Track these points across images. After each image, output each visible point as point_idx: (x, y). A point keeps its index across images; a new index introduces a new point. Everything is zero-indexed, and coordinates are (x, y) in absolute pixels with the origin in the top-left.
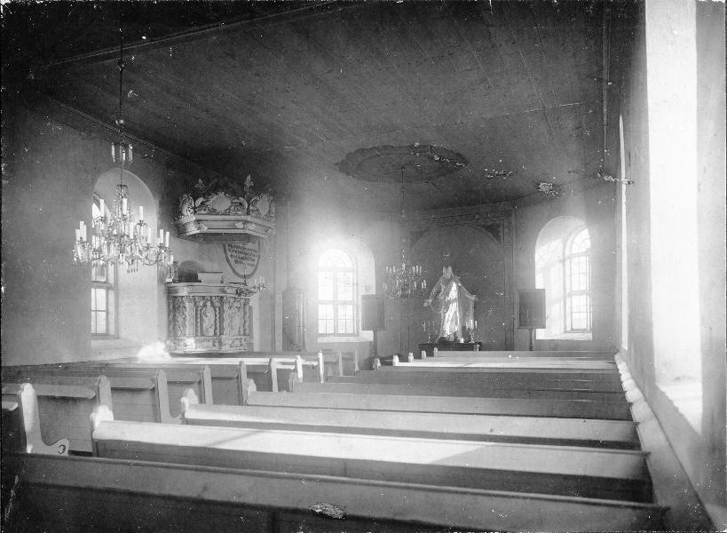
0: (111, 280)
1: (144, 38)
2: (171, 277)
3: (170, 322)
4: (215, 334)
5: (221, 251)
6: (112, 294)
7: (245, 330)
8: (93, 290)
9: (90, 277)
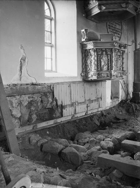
0: (53, 43)
1: (56, 163)
2: (84, 38)
3: (83, 69)
4: (108, 69)
5: (105, 27)
6: (53, 49)
7: (123, 68)
8: (45, 47)
9: (44, 41)
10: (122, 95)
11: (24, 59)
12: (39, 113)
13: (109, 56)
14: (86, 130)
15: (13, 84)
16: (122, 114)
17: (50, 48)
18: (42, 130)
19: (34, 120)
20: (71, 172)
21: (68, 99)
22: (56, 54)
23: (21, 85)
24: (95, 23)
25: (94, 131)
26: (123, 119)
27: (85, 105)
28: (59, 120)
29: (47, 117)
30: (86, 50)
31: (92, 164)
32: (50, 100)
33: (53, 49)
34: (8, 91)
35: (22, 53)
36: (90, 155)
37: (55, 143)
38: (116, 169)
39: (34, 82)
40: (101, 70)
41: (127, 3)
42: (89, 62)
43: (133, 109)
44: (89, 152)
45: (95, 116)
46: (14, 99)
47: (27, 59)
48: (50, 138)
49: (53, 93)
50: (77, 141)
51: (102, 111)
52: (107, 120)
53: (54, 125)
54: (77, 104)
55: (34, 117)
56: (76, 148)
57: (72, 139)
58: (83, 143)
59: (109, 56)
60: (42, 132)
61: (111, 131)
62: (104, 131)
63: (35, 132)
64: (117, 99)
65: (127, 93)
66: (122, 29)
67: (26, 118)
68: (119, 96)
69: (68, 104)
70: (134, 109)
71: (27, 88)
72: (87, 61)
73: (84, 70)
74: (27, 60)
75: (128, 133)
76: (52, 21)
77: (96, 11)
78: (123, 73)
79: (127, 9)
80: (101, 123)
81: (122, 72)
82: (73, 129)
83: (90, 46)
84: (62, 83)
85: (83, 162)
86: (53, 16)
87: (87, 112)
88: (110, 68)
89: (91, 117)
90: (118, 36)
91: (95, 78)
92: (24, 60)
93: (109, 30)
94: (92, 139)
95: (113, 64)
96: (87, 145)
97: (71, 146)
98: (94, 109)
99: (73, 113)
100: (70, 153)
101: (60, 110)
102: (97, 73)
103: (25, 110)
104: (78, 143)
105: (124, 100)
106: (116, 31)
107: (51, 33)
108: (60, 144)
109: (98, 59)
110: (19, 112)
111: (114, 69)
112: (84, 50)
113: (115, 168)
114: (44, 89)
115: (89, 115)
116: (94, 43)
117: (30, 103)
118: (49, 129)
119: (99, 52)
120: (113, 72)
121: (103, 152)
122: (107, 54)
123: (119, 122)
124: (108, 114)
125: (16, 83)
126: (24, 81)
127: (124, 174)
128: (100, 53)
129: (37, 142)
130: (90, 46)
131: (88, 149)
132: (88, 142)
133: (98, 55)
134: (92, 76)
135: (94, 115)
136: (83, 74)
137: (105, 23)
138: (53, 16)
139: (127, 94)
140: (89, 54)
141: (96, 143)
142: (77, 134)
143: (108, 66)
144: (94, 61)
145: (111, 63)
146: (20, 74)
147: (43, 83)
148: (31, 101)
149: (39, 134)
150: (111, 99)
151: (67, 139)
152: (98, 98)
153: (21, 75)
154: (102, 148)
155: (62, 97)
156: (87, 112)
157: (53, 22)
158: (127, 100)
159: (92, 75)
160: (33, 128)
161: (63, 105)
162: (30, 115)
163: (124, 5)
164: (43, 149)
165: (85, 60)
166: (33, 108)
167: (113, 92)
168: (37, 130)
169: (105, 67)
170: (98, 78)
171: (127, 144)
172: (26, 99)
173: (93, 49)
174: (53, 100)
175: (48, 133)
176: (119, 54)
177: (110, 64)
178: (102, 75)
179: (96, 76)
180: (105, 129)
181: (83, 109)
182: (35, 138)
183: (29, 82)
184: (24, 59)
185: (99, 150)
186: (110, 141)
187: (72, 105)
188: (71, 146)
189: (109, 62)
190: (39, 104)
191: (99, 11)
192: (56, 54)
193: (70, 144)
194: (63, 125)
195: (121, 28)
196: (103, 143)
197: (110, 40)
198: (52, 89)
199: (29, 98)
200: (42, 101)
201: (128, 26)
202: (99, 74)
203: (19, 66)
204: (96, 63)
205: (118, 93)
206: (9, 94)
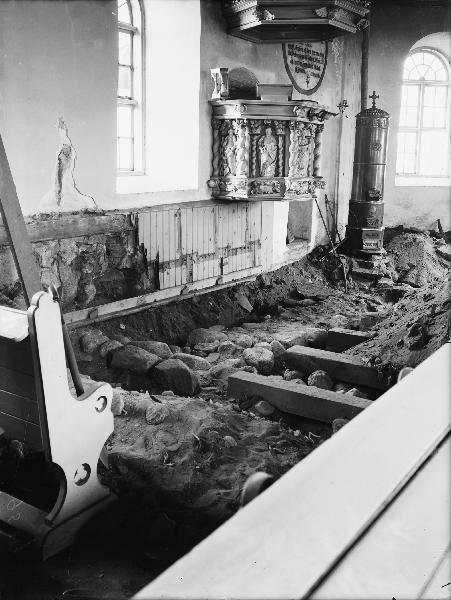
4: (277, 174)
7: (315, 169)
10: (317, 233)
11: (66, 153)
12: (102, 280)
13: (280, 139)
14: (216, 323)
15: (42, 215)
16: (314, 283)
17: (129, 109)
18: (109, 320)
19: (91, 297)
20: (170, 395)
21: (174, 246)
22: (144, 127)
23: (60, 215)
24: (250, 45)
25: (237, 323)
26: (311, 298)
27: (217, 262)
28: (150, 298)
29: (120, 289)
30: (223, 120)
31: (219, 394)
32: (130, 249)
33: (138, 112)
34: (32, 231)
35: (62, 139)
36: (218, 375)
37: (141, 350)
38: (263, 399)
39: (91, 207)
40: (260, 175)
41: (331, 8)
42: (228, 152)
43: (341, 270)
44: (218, 367)
45: (241, 288)
46: (44, 248)
47: (73, 152)
48: (127, 340)
49: (136, 231)
50: (192, 348)
51: (259, 277)
52: (273, 297)
53: (137, 310)
54: (194, 257)
55: (91, 289)
56: (185, 360)
57: (181, 343)
58: (205, 352)
59: (280, 139)
60: (111, 325)
61: (274, 326)
62: (258, 325)
63: (95, 326)
64: (305, 243)
65: (333, 229)
66: (327, 52)
67: (72, 291)
68: (310, 234)
69: (172, 258)
70: (346, 270)
71: (75, 222)
72: (224, 150)
73: (216, 173)
74: (73, 156)
75: (311, 330)
76: (135, 110)
77: (250, 21)
78: (315, 183)
79: (331, 22)
80: (256, 305)
81: (311, 179)
82: (183, 318)
83: (233, 110)
84: (160, 207)
85: (200, 390)
86: (138, 24)
87: (220, 278)
88: (281, 170)
89: (232, 291)
90: (316, 72)
91: (242, 194)
92: (68, 156)
93: (289, 58)
94: (225, 343)
95: (290, 160)
96: (213, 357)
97: (175, 358)
98: (240, 270)
99: (184, 282)
100: (174, 369)
101: (151, 272)
102: (248, 181)
103: (68, 275)
104: (195, 352)
105: (323, 247)
106: (310, 59)
107: (132, 69)
108: (152, 352)
109: (252, 146)
110: (56, 279)
111: (290, 174)
112: (217, 120)
113: (260, 398)
114: (115, 224)
115: (223, 287)
116: (243, 104)
117: (81, 260)
118: (126, 318)
119: (258, 128)
120: (287, 183)
121: (245, 370)
122: (275, 135)
123: (302, 306)
124: (276, 283)
125: (49, 212)
126: (68, 206)
127: (276, 408)
128: (258, 131)
129: (99, 347)
130: (233, 110)
131: (215, 363)
132: (216, 350)
133: (252, 135)
134: (236, 190)
135: (239, 286)
136: (212, 183)
137: (281, 45)
138: (138, 24)
139: (333, 231)
140: (231, 132)
141: (233, 354)
142: (192, 330)
143: (278, 167)
144: (241, 150)
145: (284, 158)
146: (59, 189)
147: (112, 209)
148: (83, 252)
149: (102, 329)
150: (287, 243)
151: (170, 342)
152: (251, 243)
153: (60, 192)
154: (247, 362)
155: (157, 240)
156: (220, 278)
157: (137, 39)
158: (331, 248)
159: (237, 187)
160: (89, 316)
161: (160, 261)
162: (82, 285)
163: (321, 12)
164: (113, 363)
165: (221, 146)
166: (88, 270)
167: (295, 224)
168: (97, 320)
169: (269, 169)
170: (250, 194)
171: (296, 354)
172: (71, 249)
173: (239, 119)
174: (135, 250)
175: (123, 327)
176: (307, 133)
177: (281, 162)
178: (262, 187)
179: (244, 188)
180: (261, 320)
181: (211, 269)
182: (94, 339)
183: (79, 207)
184: (66, 153)
185: (238, 366)
186: (268, 348)
187: (184, 260)
188: (175, 358)
189: (281, 156)
190: (102, 258)
191: (260, 23)
192: (144, 127)
193: (173, 351)
194: (160, 310)
195: (323, 52)
196: (249, 352)
197: (285, 101)
198: (134, 222)
199: (78, 245)
200: (108, 252)
201: (345, 43)
202: (252, 185)
203: (56, 170)
204: (247, 156)
205: (306, 229)
206: (34, 238)
